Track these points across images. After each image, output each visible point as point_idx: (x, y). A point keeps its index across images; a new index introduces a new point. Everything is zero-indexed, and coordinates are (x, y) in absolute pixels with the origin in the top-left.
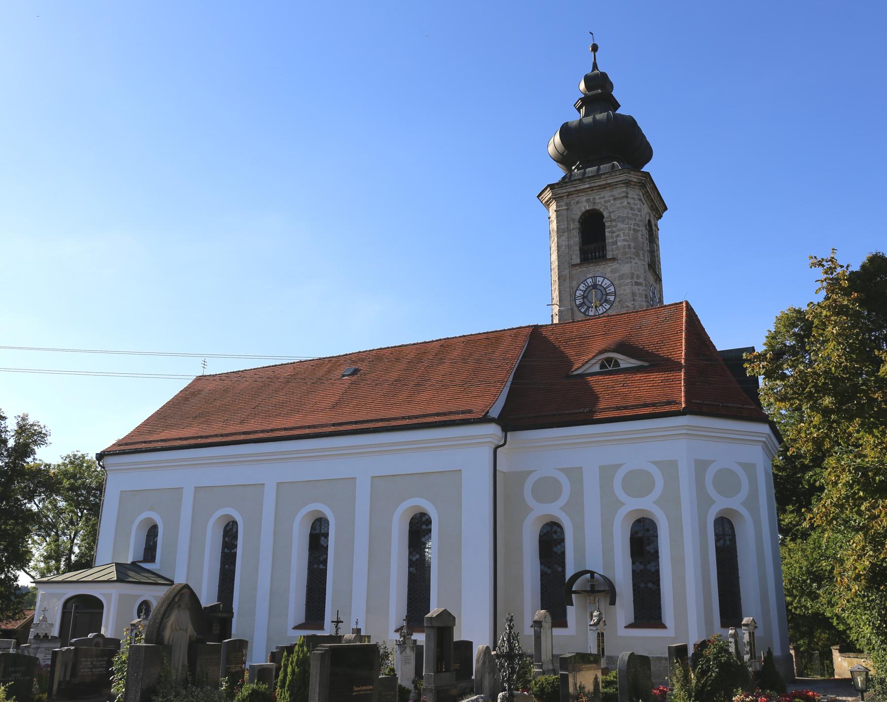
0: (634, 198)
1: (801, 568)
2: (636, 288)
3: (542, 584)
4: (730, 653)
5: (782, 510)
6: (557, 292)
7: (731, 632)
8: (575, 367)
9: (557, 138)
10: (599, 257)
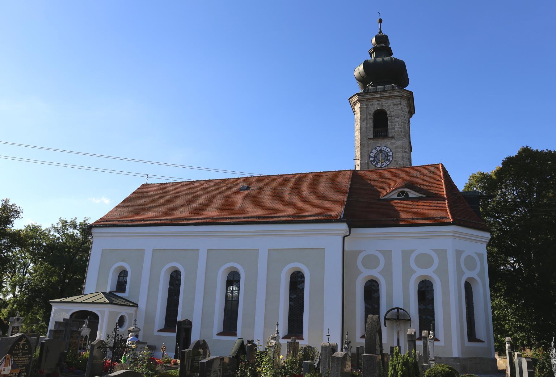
2: (404, 154)
6: (359, 153)
9: (361, 68)
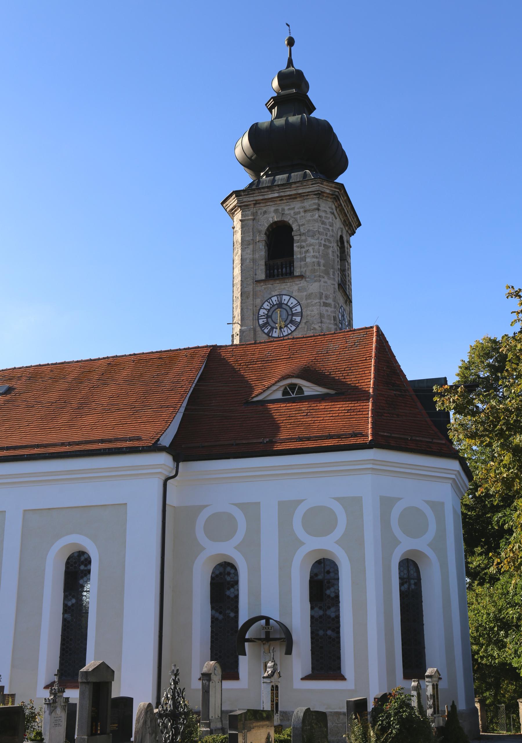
0: (325, 211)
1: (488, 614)
2: (324, 309)
3: (212, 632)
4: (412, 708)
5: (470, 552)
7: (414, 684)
8: (256, 393)
10: (286, 274)
